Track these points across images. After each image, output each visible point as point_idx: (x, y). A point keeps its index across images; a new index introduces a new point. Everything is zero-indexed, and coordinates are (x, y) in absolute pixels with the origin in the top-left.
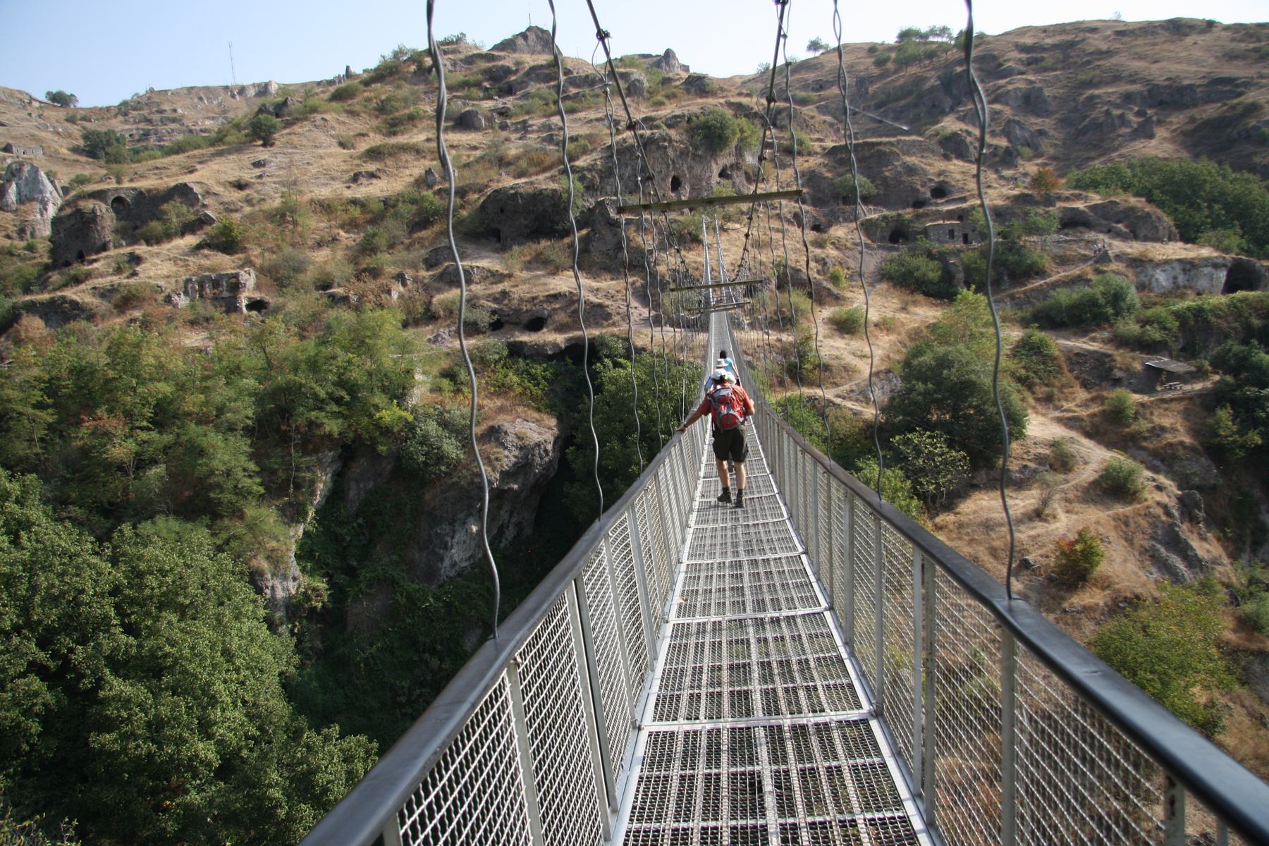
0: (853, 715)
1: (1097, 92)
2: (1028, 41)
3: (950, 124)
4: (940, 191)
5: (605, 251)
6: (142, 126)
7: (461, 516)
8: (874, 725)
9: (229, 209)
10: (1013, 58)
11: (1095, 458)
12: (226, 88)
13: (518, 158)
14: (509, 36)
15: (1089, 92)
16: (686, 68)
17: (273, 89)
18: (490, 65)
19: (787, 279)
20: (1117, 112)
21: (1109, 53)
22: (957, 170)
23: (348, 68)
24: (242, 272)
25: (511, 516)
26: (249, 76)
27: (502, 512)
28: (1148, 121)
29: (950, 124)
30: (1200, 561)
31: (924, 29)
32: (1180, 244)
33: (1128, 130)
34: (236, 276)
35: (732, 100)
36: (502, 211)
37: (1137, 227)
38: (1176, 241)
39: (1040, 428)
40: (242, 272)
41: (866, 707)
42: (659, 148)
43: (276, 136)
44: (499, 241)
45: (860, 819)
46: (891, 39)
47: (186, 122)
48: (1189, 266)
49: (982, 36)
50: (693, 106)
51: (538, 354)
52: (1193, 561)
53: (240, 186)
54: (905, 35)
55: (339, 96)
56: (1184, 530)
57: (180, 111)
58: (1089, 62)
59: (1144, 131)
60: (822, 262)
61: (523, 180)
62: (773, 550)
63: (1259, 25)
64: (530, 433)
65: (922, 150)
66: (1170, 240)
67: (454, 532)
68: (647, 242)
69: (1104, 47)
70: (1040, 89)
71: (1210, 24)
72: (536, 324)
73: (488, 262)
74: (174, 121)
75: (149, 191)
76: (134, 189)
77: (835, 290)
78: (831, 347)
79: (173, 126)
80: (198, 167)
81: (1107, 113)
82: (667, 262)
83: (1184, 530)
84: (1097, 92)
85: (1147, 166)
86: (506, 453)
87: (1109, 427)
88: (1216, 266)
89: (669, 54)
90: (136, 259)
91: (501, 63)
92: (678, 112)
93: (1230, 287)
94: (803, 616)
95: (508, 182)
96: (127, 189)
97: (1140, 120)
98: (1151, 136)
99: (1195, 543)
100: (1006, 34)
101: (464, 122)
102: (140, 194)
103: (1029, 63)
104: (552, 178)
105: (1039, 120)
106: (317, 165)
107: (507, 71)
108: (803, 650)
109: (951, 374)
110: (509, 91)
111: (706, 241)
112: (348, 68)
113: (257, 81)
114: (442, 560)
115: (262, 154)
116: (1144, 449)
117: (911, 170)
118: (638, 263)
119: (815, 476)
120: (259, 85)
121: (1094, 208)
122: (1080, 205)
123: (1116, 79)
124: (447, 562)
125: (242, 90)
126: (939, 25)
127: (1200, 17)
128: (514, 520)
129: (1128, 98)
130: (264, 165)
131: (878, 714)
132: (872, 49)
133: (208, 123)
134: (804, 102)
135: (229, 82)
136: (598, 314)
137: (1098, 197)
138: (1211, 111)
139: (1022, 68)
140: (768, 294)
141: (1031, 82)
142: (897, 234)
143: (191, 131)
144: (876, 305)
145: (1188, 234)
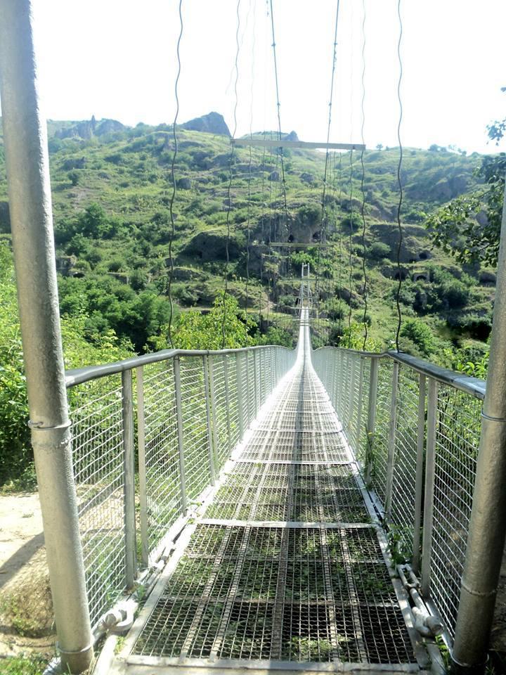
23: (93, 117)
36: (204, 243)
68: (275, 268)
107: (204, 156)
110: (205, 167)
112: (93, 117)
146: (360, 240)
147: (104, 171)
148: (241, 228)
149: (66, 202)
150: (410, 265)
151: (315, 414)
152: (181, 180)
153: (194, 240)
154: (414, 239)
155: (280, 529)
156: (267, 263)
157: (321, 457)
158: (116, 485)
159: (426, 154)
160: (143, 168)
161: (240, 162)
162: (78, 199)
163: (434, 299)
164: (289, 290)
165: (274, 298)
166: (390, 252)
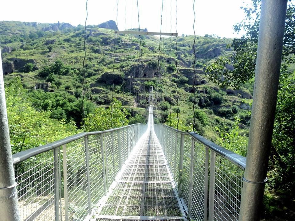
23: (59, 22)
36: (107, 77)
68: (138, 88)
112: (59, 22)
125: (29, 24)
142: (192, 91)
146: (175, 76)
153: (103, 76)
162: (52, 58)
164: (144, 98)
165: (138, 101)
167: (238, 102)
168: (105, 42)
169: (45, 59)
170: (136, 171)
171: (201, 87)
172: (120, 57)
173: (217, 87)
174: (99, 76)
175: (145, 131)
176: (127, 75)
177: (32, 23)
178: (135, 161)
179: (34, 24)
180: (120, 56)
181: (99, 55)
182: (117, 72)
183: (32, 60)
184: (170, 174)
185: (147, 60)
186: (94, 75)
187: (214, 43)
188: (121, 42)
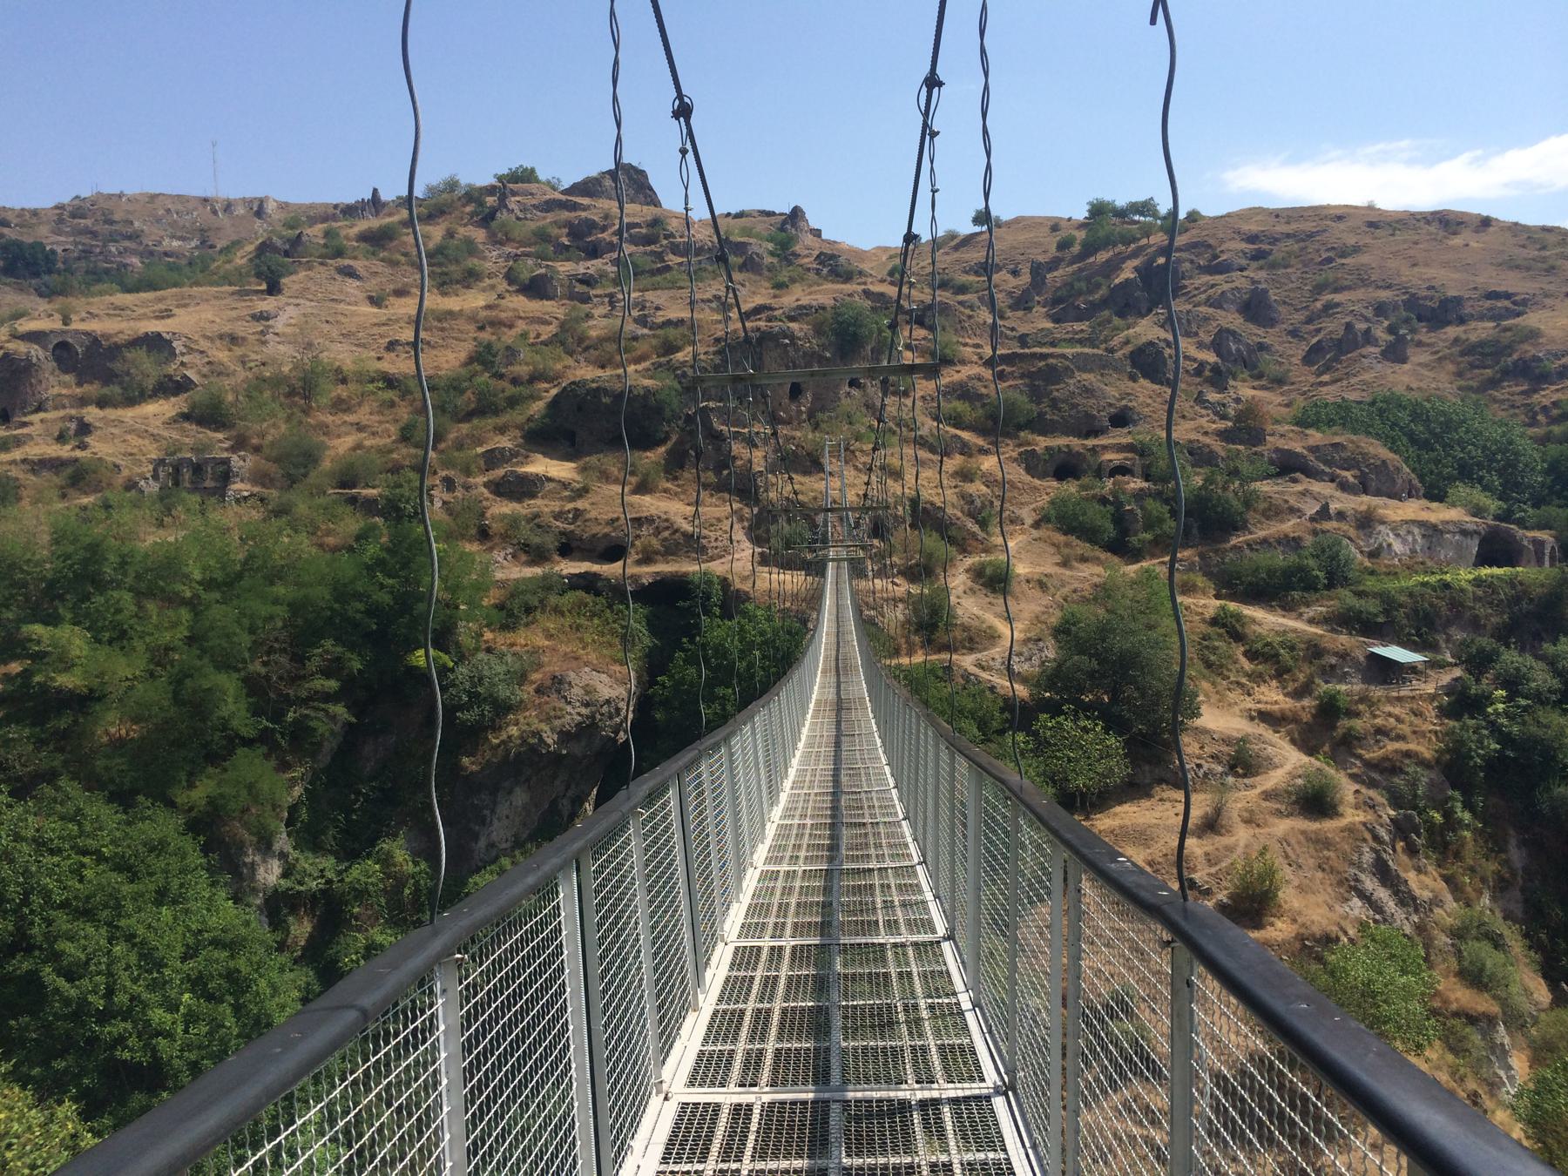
0: (973, 1089)
1: (1338, 298)
2: (1252, 227)
3: (1146, 330)
4: (1121, 419)
5: (698, 455)
6: (85, 240)
7: (507, 784)
8: (999, 1103)
9: (216, 370)
10: (1234, 248)
11: (1289, 762)
12: (206, 200)
13: (602, 340)
14: (594, 173)
15: (1328, 297)
16: (817, 233)
17: (270, 207)
18: (573, 214)
19: (924, 516)
20: (1361, 326)
21: (1356, 250)
22: (1145, 394)
23: (375, 191)
24: (235, 458)
25: (568, 788)
26: (235, 185)
27: (557, 783)
28: (1401, 340)
29: (1146, 330)
30: (1414, 899)
31: (1121, 202)
32: (1424, 502)
33: (1377, 350)
34: (226, 462)
35: (872, 288)
36: (580, 409)
37: (1373, 480)
38: (1418, 498)
39: (1219, 718)
40: (235, 458)
41: (916, 860)
42: (778, 345)
43: (284, 280)
44: (573, 444)
45: (922, 1003)
46: (1081, 213)
47: (145, 242)
48: (1433, 531)
49: (1193, 216)
50: (825, 294)
51: (616, 593)
52: (1406, 899)
53: (234, 340)
54: (1099, 210)
55: (377, 240)
56: (1399, 861)
57: (136, 224)
58: (1329, 260)
59: (1395, 353)
60: (967, 499)
61: (608, 372)
62: (880, 858)
63: (1545, 229)
64: (600, 687)
65: (1101, 365)
66: (1410, 496)
67: (495, 803)
68: (758, 459)
69: (1351, 240)
70: (1265, 291)
71: (1486, 222)
72: (615, 552)
73: (560, 470)
74: (129, 238)
75: (107, 336)
76: (87, 334)
77: (981, 535)
78: (969, 606)
79: (127, 244)
80: (176, 311)
81: (1349, 326)
82: (779, 489)
83: (1399, 861)
84: (1338, 298)
85: (416, 855)
86: (569, 708)
87: (1323, 729)
88: (1465, 533)
89: (796, 214)
90: (84, 428)
91: (583, 214)
92: (805, 301)
93: (1484, 559)
94: (955, 1101)
95: (586, 373)
96: (77, 332)
97: (1391, 338)
98: (1404, 360)
99: (1411, 877)
100: (1229, 215)
101: (536, 288)
102: (94, 340)
103: (1258, 256)
104: (646, 373)
105: (1261, 332)
106: (335, 322)
107: (591, 226)
108: (913, 992)
109: (1119, 643)
110: (594, 252)
111: (828, 468)
112: (375, 191)
113: (249, 195)
114: (476, 838)
115: (268, 304)
116: (1359, 757)
117: (1088, 391)
118: (744, 488)
119: (937, 756)
120: (251, 201)
121: (1314, 449)
122: (1298, 448)
123: (1364, 282)
124: (482, 843)
125: (228, 206)
126: (1140, 197)
127: (1475, 211)
128: (570, 793)
129: (1381, 309)
130: (267, 319)
131: (950, 937)
132: (1055, 226)
133: (176, 243)
134: (962, 289)
135: (210, 193)
136: (691, 544)
137: (1319, 435)
138: (1481, 331)
139: (1244, 262)
140: (903, 534)
141: (1254, 282)
142: (1065, 468)
143: (151, 253)
144: (1025, 553)
145: (1436, 494)
146: (962, 392)
147: (351, 262)
148: (671, 368)
149: (247, 329)
150: (1090, 442)
151: (882, 886)
152: (534, 280)
153: (555, 403)
154: (1089, 378)
155: (804, 1103)
156: (737, 448)
157: (892, 926)
158: (378, 1072)
159: (1081, 226)
160: (446, 257)
161: (672, 235)
162: (279, 324)
163: (1161, 521)
164: (796, 509)
165: (757, 534)
166: (1028, 411)
167: (1341, 515)
168: (584, 241)
169: (241, 329)
170: (806, 841)
171: (1111, 446)
172: (658, 308)
173: (1207, 440)
174: (537, 408)
175: (1310, 820)
176: (690, 388)
177: (248, 202)
178: (798, 812)
179: (258, 209)
180: (657, 302)
181: (548, 306)
182: (638, 376)
183: (159, 334)
184: (933, 907)
185: (804, 307)
186: (513, 402)
187: (1144, 241)
188: (666, 237)
